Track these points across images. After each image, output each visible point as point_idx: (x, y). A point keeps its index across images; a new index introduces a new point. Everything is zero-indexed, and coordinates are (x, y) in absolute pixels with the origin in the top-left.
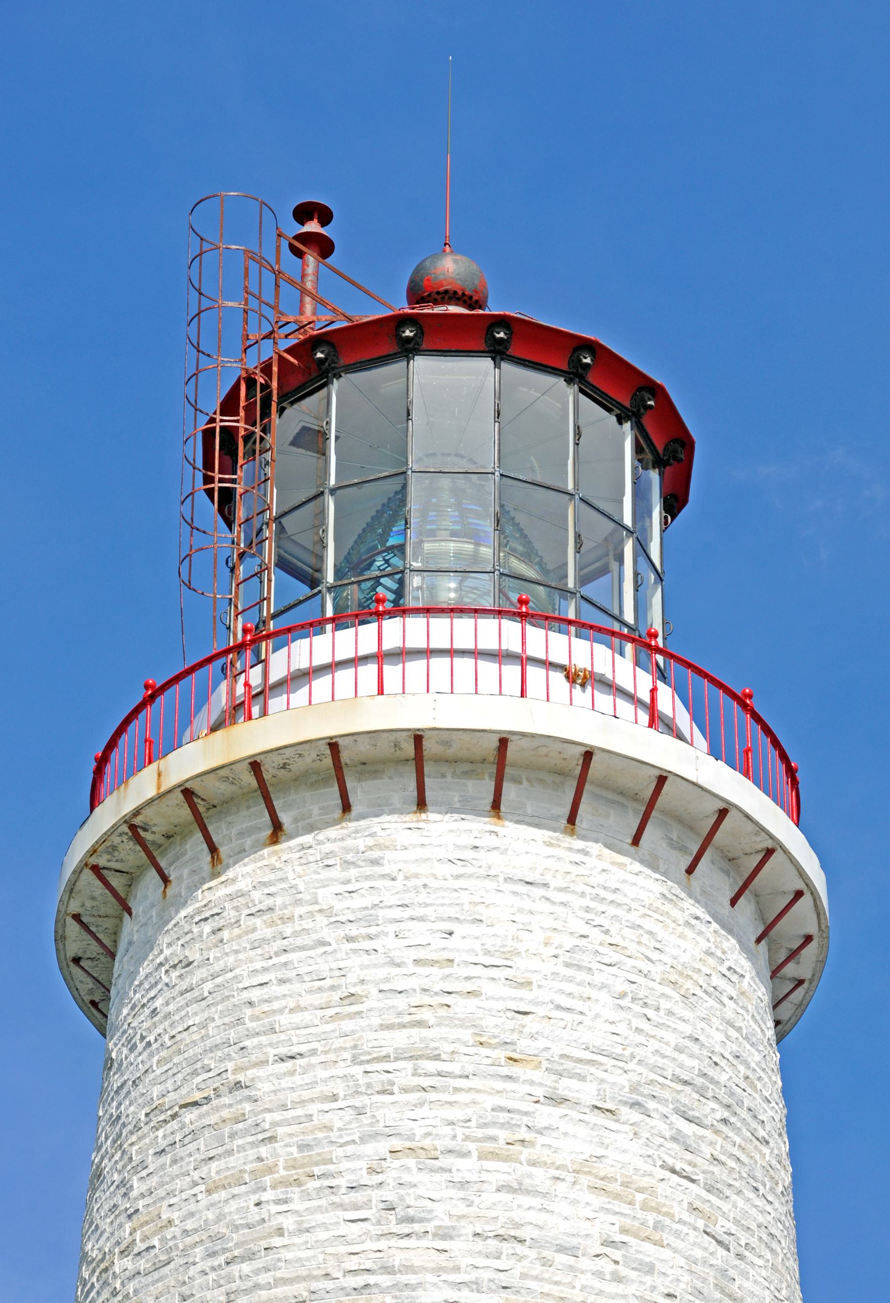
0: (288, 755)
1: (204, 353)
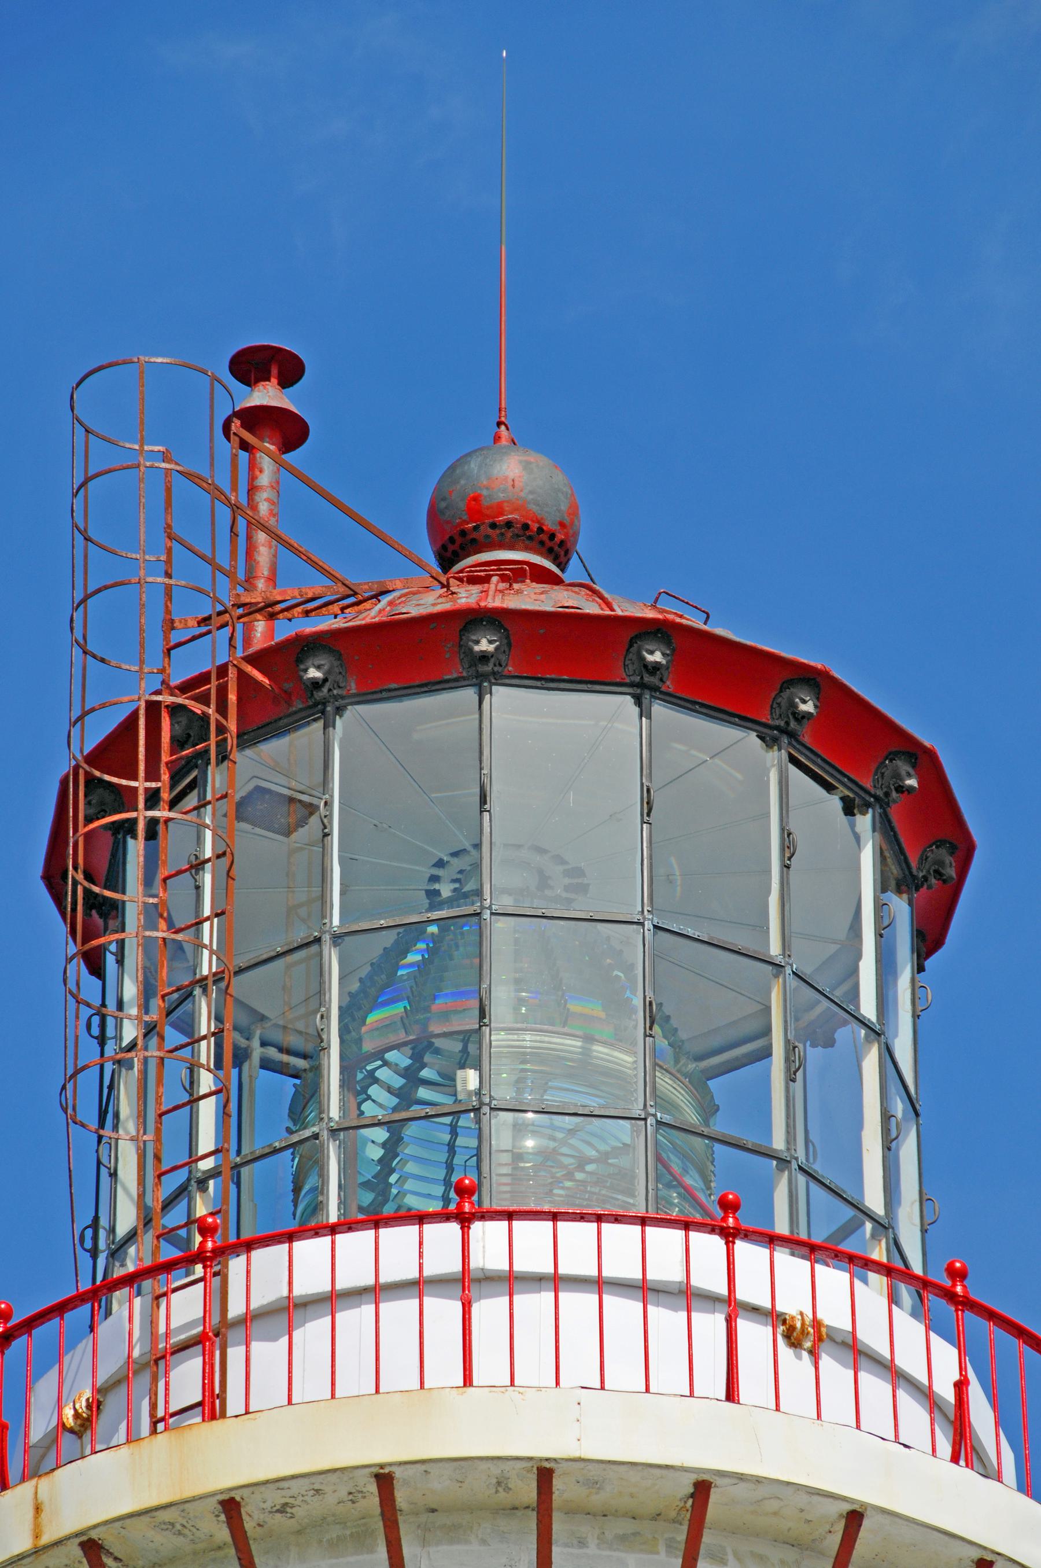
0: (294, 1491)
1: (94, 656)
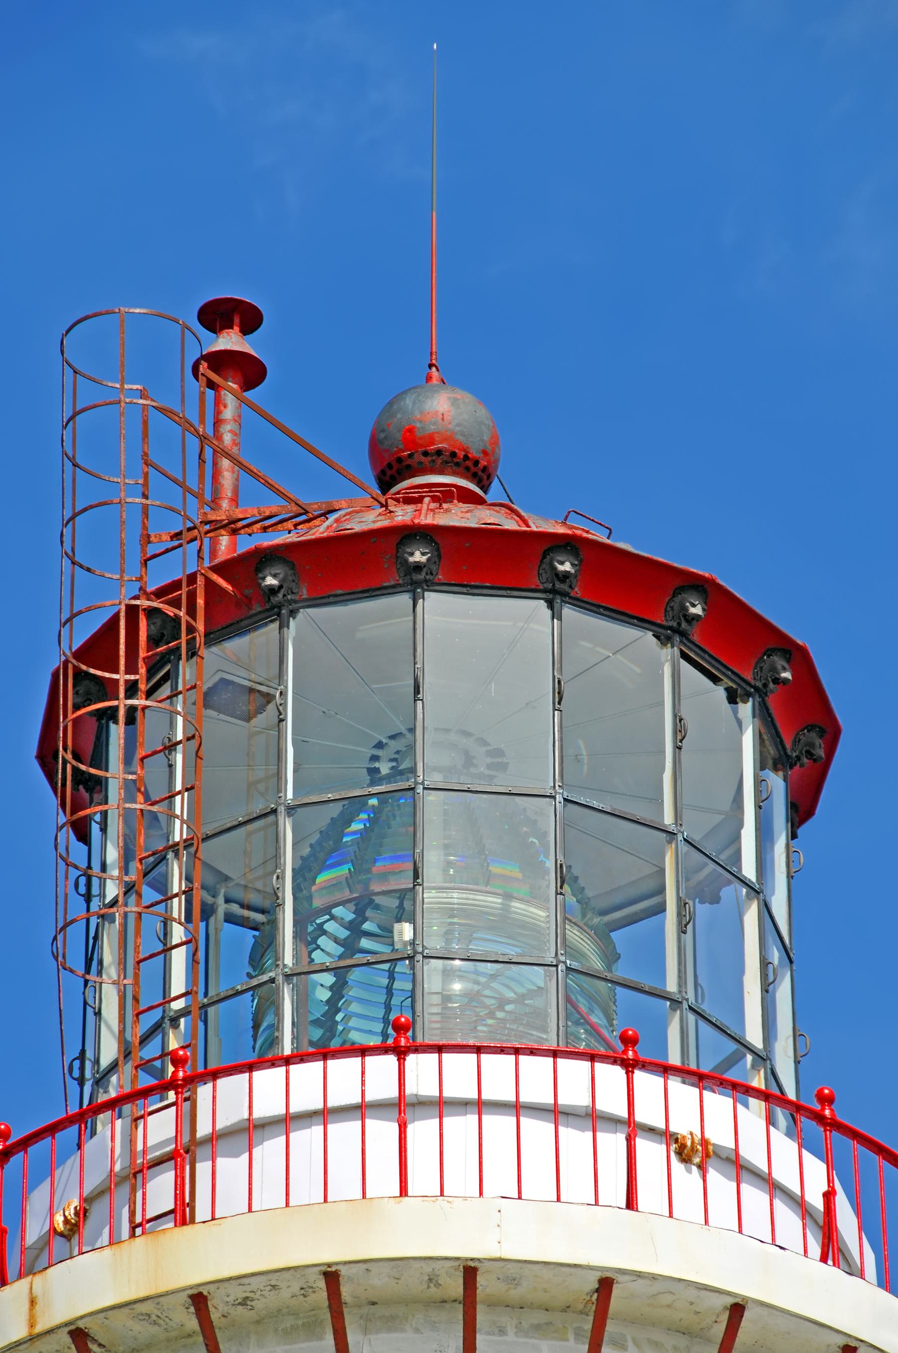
0: (254, 1287)
1: (81, 566)
